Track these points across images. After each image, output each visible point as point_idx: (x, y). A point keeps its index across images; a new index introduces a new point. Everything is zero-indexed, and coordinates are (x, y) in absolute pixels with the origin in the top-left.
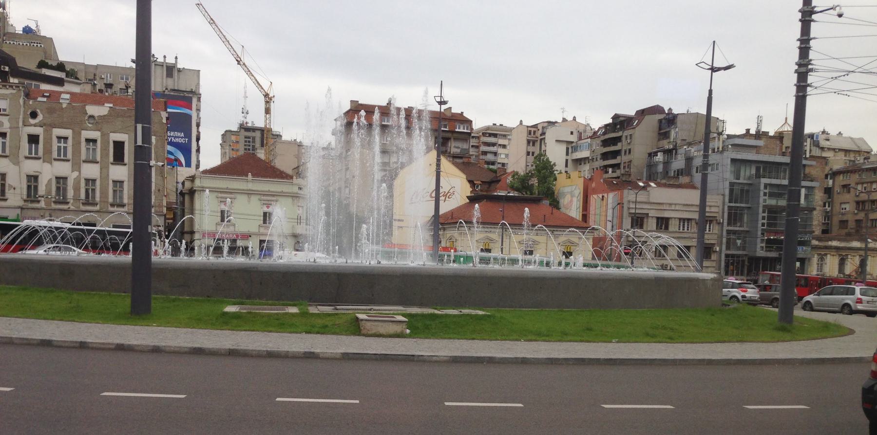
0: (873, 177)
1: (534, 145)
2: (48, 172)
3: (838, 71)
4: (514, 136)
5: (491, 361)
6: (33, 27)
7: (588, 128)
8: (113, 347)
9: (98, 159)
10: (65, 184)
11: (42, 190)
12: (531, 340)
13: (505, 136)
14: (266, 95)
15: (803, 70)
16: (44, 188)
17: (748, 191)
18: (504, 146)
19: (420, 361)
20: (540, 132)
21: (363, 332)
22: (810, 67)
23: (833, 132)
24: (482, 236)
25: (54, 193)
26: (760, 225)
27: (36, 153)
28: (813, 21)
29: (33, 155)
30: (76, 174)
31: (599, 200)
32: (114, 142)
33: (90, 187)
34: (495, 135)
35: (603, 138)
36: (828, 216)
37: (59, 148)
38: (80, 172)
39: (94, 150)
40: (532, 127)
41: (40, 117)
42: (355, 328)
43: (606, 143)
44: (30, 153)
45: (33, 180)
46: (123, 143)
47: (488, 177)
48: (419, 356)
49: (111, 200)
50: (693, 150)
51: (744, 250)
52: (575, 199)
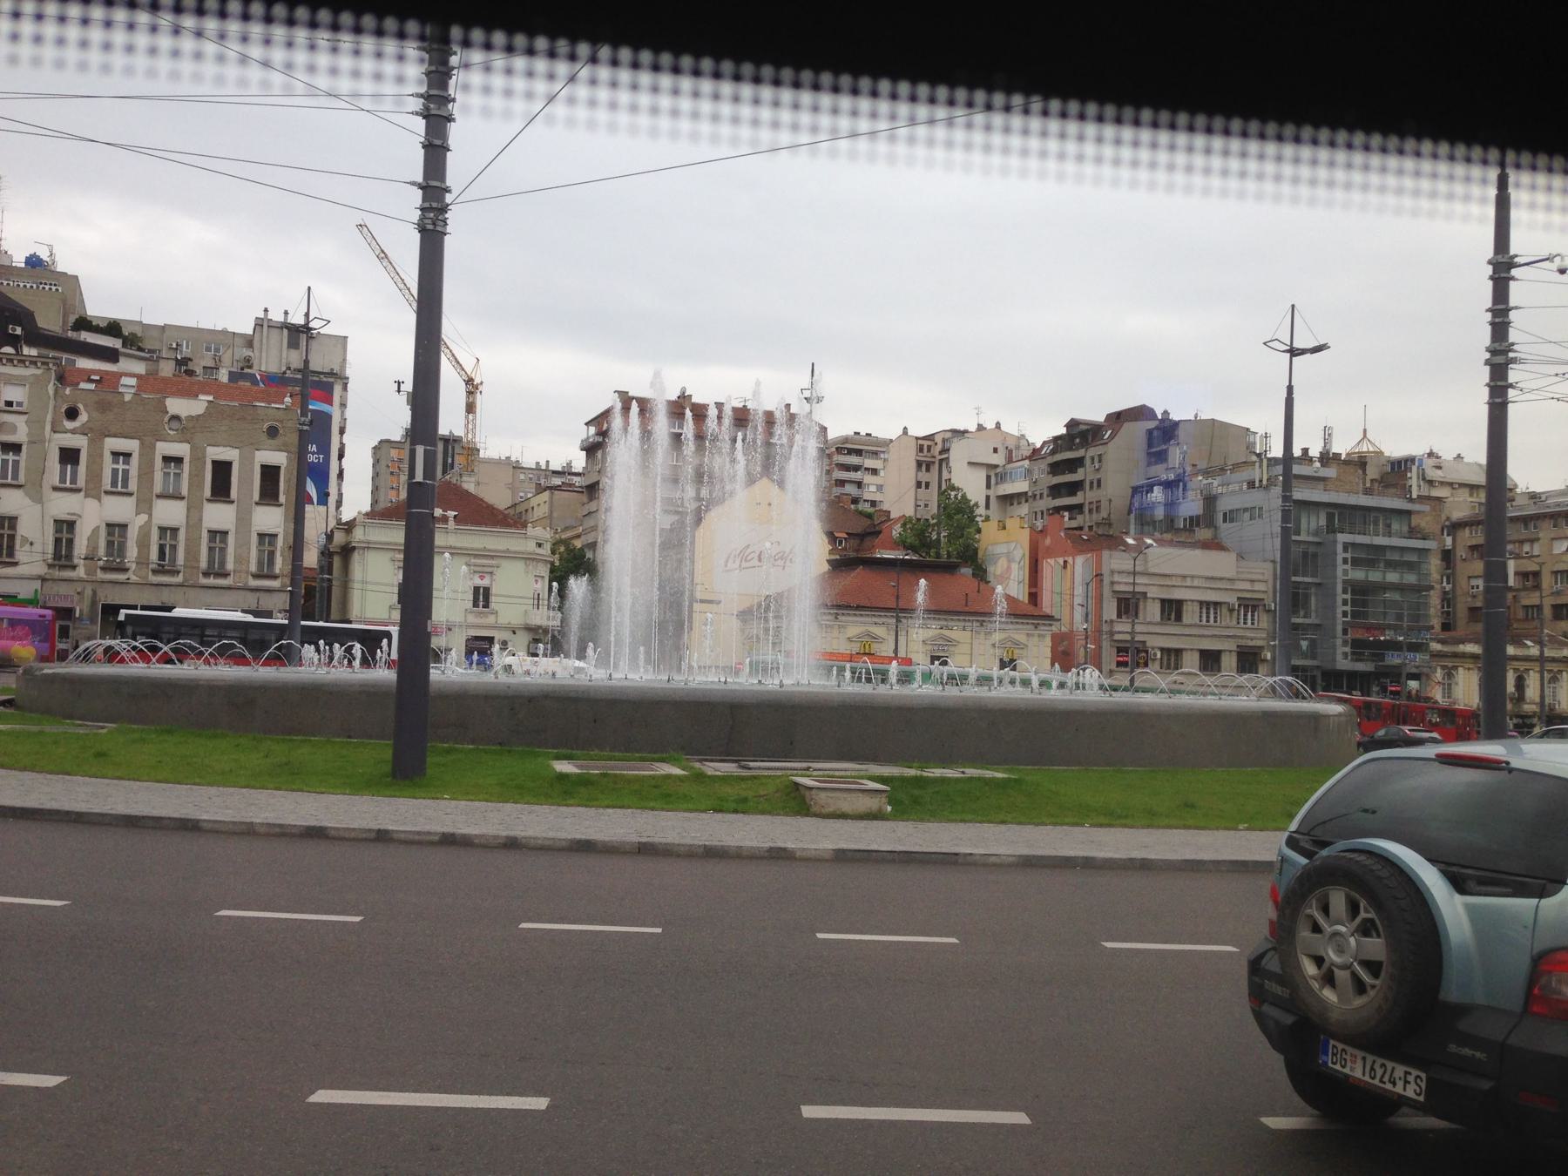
1: (928, 470)
2: (92, 515)
3: (1553, 363)
4: (893, 454)
6: (44, 256)
7: (1023, 443)
8: (373, 835)
9: (185, 492)
10: (123, 535)
11: (81, 548)
12: (1101, 826)
13: (876, 453)
14: (469, 381)
15: (1500, 359)
16: (85, 542)
17: (1315, 555)
18: (875, 472)
19: (969, 864)
20: (939, 447)
21: (814, 809)
22: (1511, 355)
23: (1447, 455)
24: (931, 633)
25: (102, 551)
26: (1339, 615)
27: (74, 481)
28: (1513, 278)
29: (68, 485)
30: (143, 518)
31: (1058, 569)
32: (214, 462)
33: (65, 535)
34: (859, 452)
36: (1448, 599)
37: (115, 472)
38: (150, 515)
39: (178, 475)
40: (924, 438)
41: (83, 417)
42: (797, 802)
43: (1055, 468)
44: (63, 480)
45: (65, 527)
46: (229, 464)
47: (860, 526)
48: (966, 855)
49: (204, 564)
50: (1216, 483)
51: (1314, 658)
52: (1015, 566)
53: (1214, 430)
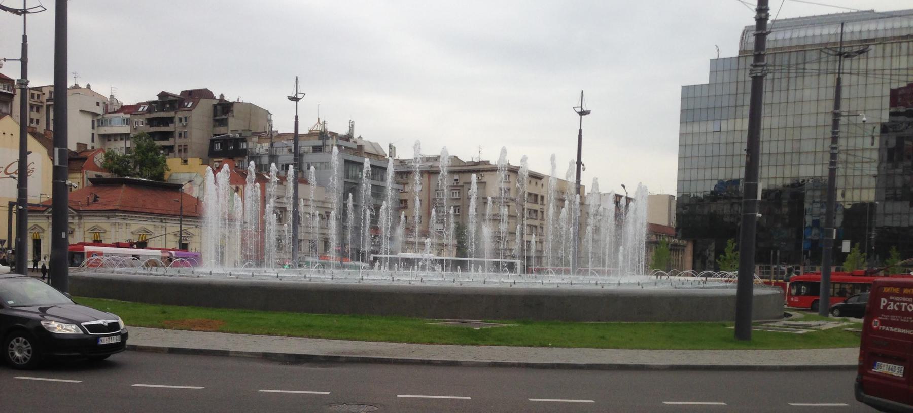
0: (910, 300)
1: (38, 111)
5: (224, 354)
35: (148, 116)
53: (252, 110)
